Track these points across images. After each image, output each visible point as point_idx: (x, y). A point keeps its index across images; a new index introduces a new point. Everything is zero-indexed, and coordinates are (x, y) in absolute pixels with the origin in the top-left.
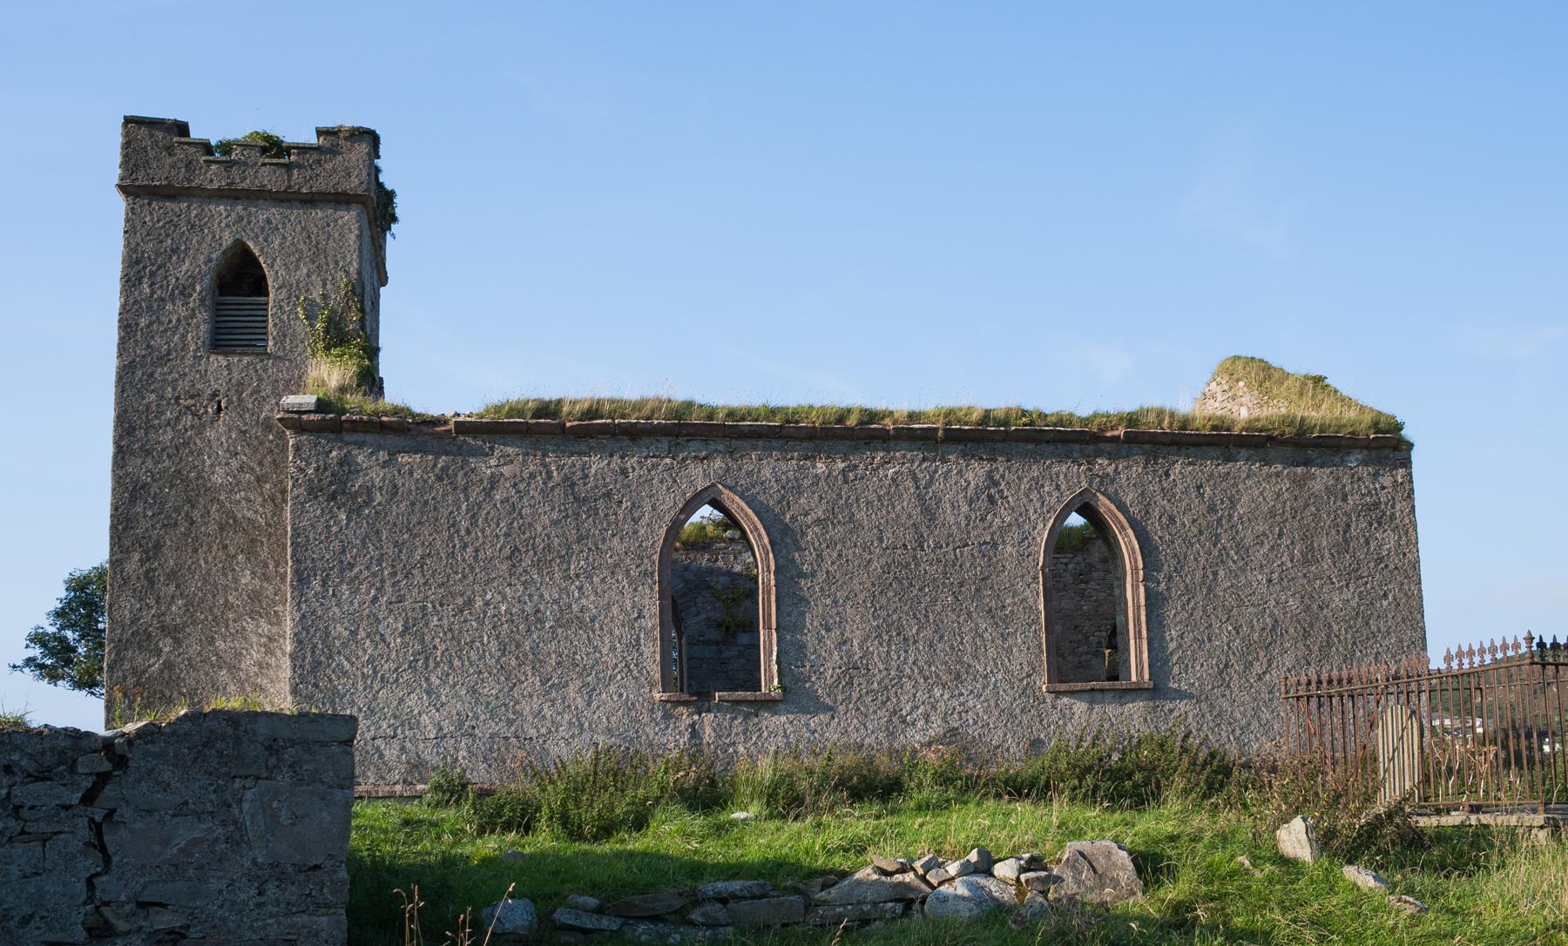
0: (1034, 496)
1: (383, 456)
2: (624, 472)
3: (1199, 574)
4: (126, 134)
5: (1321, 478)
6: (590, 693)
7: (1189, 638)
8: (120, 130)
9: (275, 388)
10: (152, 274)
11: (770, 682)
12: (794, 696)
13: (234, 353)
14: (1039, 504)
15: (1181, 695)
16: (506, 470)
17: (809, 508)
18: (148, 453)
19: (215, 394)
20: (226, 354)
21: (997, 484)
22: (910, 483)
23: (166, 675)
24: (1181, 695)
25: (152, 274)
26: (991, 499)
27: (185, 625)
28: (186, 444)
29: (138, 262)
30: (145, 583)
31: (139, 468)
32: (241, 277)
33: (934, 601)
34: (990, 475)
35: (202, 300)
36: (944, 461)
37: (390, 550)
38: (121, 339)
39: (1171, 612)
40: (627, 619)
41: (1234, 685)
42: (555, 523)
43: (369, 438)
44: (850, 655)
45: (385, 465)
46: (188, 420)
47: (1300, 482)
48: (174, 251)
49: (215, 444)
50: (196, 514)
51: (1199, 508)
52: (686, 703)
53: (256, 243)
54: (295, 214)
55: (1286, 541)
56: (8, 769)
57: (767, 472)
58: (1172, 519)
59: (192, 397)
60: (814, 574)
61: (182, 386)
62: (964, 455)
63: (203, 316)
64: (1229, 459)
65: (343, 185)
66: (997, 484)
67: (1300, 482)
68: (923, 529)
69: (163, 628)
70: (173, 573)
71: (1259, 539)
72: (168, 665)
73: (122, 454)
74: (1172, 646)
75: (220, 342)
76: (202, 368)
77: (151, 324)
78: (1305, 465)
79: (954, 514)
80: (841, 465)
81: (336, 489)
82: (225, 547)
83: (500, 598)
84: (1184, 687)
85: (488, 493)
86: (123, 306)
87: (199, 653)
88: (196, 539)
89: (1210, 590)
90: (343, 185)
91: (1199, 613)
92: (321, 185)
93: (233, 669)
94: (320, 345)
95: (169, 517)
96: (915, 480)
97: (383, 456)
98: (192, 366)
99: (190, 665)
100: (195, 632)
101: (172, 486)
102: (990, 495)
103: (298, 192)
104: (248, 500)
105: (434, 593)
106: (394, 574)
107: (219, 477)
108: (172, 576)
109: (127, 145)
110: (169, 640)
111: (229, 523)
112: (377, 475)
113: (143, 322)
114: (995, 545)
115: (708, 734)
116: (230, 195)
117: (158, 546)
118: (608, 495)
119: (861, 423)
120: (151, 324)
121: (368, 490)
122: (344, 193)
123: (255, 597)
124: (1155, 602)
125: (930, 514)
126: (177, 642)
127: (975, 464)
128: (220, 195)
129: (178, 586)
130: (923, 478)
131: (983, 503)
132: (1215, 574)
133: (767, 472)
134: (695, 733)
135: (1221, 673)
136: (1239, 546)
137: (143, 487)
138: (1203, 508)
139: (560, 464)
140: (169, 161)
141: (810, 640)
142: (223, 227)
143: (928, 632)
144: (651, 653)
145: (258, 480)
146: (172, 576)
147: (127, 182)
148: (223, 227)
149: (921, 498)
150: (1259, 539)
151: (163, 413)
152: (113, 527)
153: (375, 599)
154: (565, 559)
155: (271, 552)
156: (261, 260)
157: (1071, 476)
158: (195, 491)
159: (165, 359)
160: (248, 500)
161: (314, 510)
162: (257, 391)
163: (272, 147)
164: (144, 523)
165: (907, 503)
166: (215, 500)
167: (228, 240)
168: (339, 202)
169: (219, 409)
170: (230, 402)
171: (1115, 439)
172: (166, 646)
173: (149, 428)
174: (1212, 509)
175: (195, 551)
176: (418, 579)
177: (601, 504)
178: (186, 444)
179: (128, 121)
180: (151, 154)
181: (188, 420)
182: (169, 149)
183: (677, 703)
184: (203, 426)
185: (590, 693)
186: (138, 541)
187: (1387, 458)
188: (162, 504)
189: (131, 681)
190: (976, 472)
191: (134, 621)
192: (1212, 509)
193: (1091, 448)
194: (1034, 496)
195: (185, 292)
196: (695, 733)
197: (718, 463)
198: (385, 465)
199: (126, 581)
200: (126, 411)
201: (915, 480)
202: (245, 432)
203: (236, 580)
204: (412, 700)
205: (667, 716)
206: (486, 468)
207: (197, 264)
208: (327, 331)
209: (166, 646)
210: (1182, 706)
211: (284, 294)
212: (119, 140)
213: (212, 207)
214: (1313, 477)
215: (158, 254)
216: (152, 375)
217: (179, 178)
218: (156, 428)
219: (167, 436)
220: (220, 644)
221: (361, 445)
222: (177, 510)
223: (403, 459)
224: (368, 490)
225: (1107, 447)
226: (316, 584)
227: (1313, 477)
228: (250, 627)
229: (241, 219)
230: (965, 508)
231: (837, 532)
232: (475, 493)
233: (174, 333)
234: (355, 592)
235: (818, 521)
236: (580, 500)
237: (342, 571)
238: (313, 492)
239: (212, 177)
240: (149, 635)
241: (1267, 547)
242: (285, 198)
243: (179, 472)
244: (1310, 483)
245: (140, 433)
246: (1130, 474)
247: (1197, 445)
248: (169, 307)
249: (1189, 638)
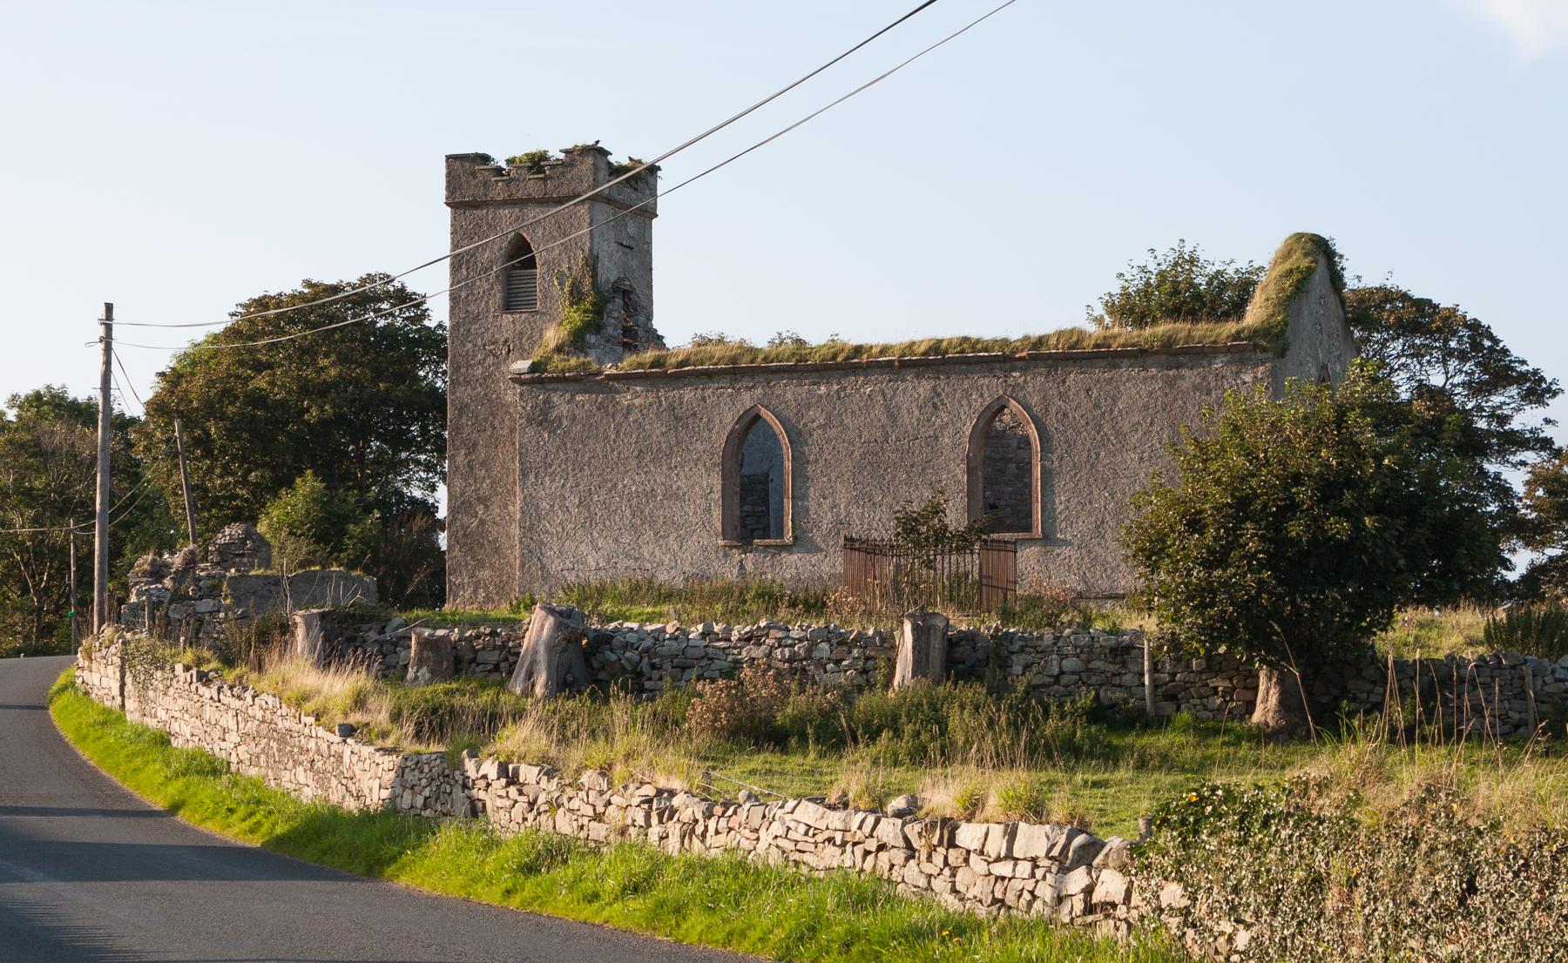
0: (964, 402)
1: (568, 396)
2: (704, 399)
3: (1085, 454)
4: (448, 167)
5: (1190, 377)
6: (681, 541)
7: (1074, 502)
8: (444, 164)
11: (1038, 530)
12: (800, 542)
14: (966, 403)
15: (1067, 543)
16: (637, 402)
17: (816, 416)
18: (468, 383)
21: (939, 395)
22: (880, 398)
24: (1067, 543)
26: (935, 407)
32: (520, 254)
33: (894, 478)
34: (934, 389)
36: (904, 380)
37: (572, 455)
39: (1060, 484)
40: (702, 490)
41: (1109, 536)
42: (663, 434)
43: (560, 386)
44: (838, 514)
45: (569, 402)
46: (490, 360)
47: (1171, 383)
50: (496, 423)
51: (1086, 405)
52: (736, 547)
55: (1156, 428)
56: (1386, 959)
57: (789, 395)
58: (1065, 415)
60: (816, 461)
61: (488, 336)
62: (917, 376)
63: (498, 287)
64: (1115, 367)
66: (939, 395)
67: (1171, 383)
68: (889, 429)
71: (1135, 427)
72: (482, 522)
74: (1062, 507)
75: (509, 306)
78: (1177, 368)
79: (910, 417)
80: (836, 387)
81: (542, 418)
83: (631, 482)
84: (1069, 537)
85: (626, 417)
89: (1092, 466)
91: (1082, 484)
96: (884, 395)
97: (568, 396)
100: (496, 500)
102: (934, 403)
105: (596, 480)
108: (483, 464)
109: (448, 175)
114: (937, 438)
115: (749, 566)
117: (475, 445)
118: (694, 414)
119: (847, 358)
121: (559, 418)
124: (1047, 475)
125: (893, 418)
126: (486, 507)
127: (924, 382)
128: (504, 203)
130: (889, 393)
131: (929, 408)
132: (1098, 454)
133: (789, 395)
134: (742, 567)
135: (1097, 527)
136: (1118, 434)
138: (1090, 405)
139: (668, 395)
141: (812, 505)
142: (507, 223)
143: (889, 499)
144: (717, 513)
146: (483, 464)
148: (507, 223)
149: (887, 407)
150: (1135, 427)
157: (988, 388)
159: (476, 319)
161: (530, 432)
162: (530, 337)
164: (467, 431)
165: (878, 411)
166: (507, 412)
171: (1021, 359)
172: (480, 510)
173: (468, 366)
174: (1097, 406)
176: (587, 472)
177: (690, 421)
179: (448, 157)
181: (490, 360)
182: (474, 174)
183: (731, 547)
185: (681, 541)
186: (463, 442)
187: (1249, 359)
189: (460, 534)
190: (924, 387)
192: (1097, 406)
193: (1008, 365)
194: (964, 402)
196: (742, 567)
198: (569, 402)
201: (884, 395)
204: (582, 547)
205: (726, 555)
206: (625, 399)
207: (494, 244)
208: (571, 293)
209: (480, 510)
210: (1066, 551)
211: (545, 268)
212: (444, 171)
214: (1183, 378)
219: (479, 371)
221: (555, 391)
222: (486, 420)
223: (579, 398)
224: (559, 418)
225: (1020, 364)
226: (532, 477)
227: (1183, 378)
230: (917, 413)
231: (832, 433)
232: (619, 418)
235: (820, 427)
236: (677, 418)
238: (530, 421)
239: (499, 191)
241: (1140, 433)
242: (544, 202)
244: (1180, 382)
245: (463, 370)
246: (1035, 384)
249: (1074, 502)
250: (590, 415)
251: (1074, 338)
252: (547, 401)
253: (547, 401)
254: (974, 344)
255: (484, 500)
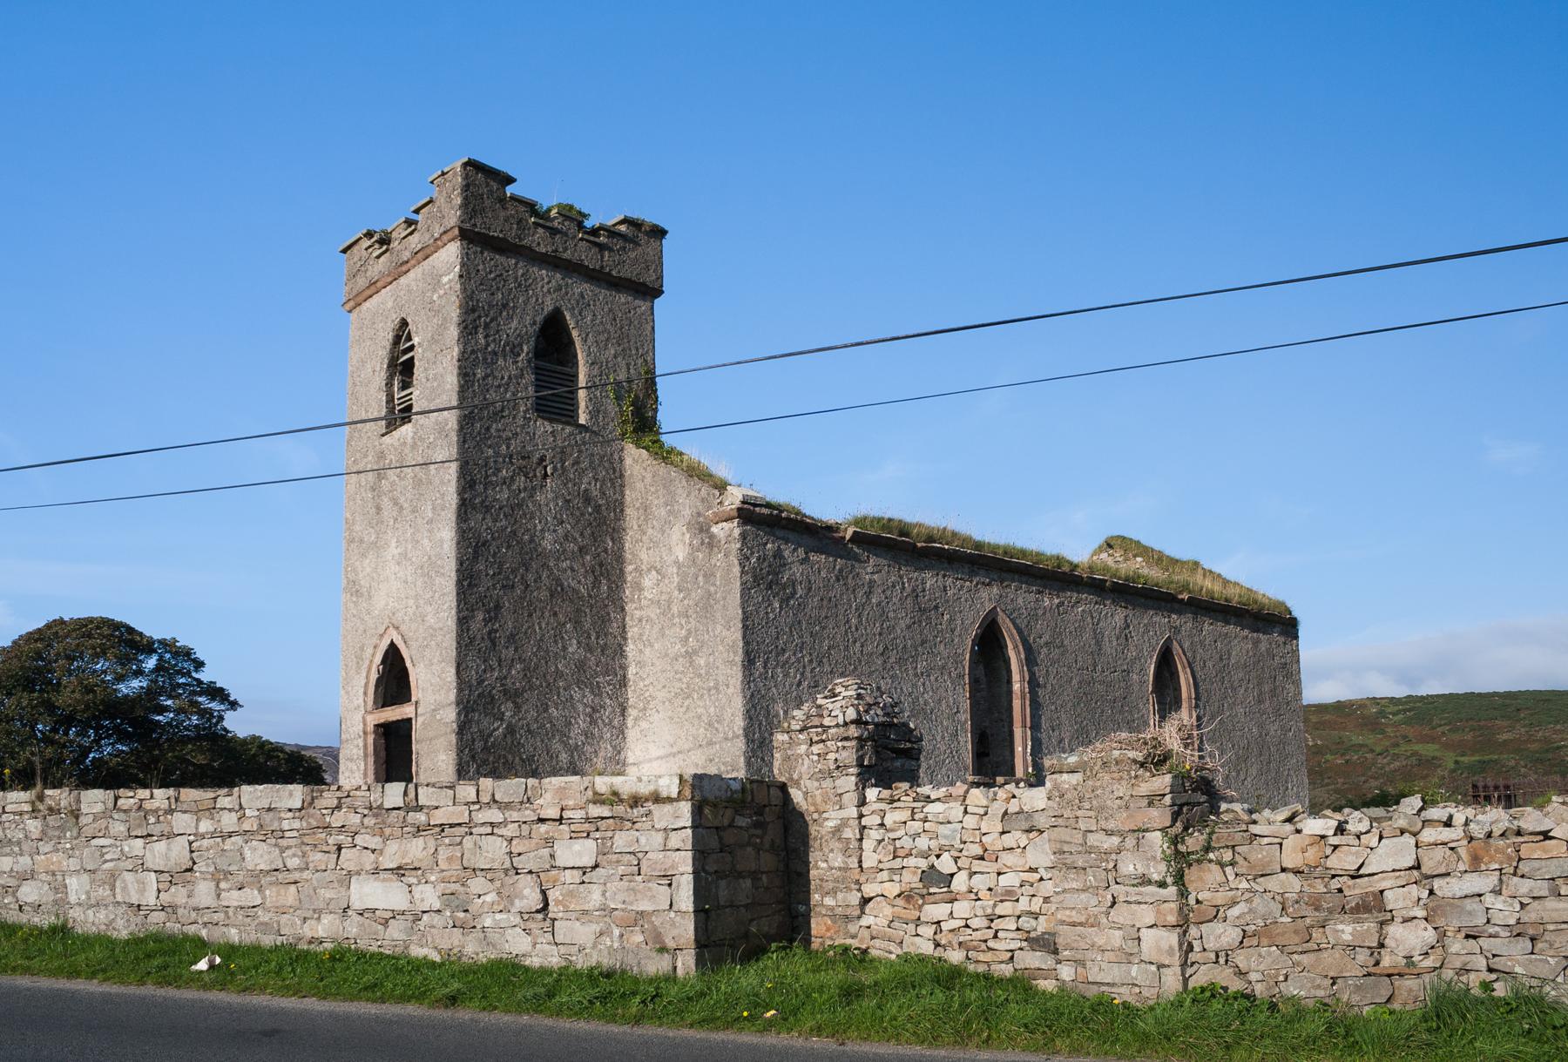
9: (591, 462)
10: (487, 326)
13: (559, 421)
18: (488, 509)
19: (542, 459)
20: (551, 421)
23: (509, 739)
25: (487, 326)
27: (524, 691)
28: (520, 506)
29: (473, 310)
30: (488, 643)
31: (475, 519)
32: (553, 342)
35: (529, 361)
37: (807, 639)
38: (461, 386)
46: (521, 481)
47: (1256, 643)
48: (505, 306)
49: (545, 509)
50: (530, 577)
53: (573, 315)
54: (603, 293)
59: (523, 458)
65: (624, 264)
67: (1256, 643)
69: (505, 692)
70: (512, 636)
72: (511, 730)
73: (465, 509)
76: (531, 430)
77: (487, 376)
80: (1057, 601)
82: (555, 614)
85: (868, 594)
86: (463, 353)
87: (536, 720)
88: (530, 603)
90: (624, 264)
92: (627, 272)
93: (565, 736)
94: (630, 428)
95: (507, 578)
98: (523, 427)
99: (529, 731)
100: (532, 697)
101: (508, 547)
103: (609, 274)
104: (573, 570)
106: (811, 661)
107: (548, 543)
108: (512, 638)
110: (510, 705)
111: (558, 591)
112: (797, 571)
113: (480, 373)
116: (553, 262)
117: (498, 607)
118: (936, 607)
120: (487, 376)
121: (793, 583)
122: (644, 284)
123: (581, 666)
126: (518, 707)
129: (516, 650)
137: (484, 545)
139: (911, 576)
140: (502, 214)
142: (546, 291)
145: (581, 549)
147: (467, 226)
151: (499, 470)
152: (459, 583)
153: (799, 684)
154: (915, 659)
155: (593, 624)
156: (575, 333)
158: (530, 555)
159: (498, 415)
160: (573, 570)
163: (574, 217)
167: (549, 307)
168: (637, 292)
169: (546, 475)
170: (555, 469)
172: (508, 710)
175: (530, 615)
176: (827, 668)
178: (520, 506)
180: (487, 203)
184: (534, 488)
188: (501, 565)
189: (479, 745)
191: (480, 682)
195: (515, 351)
197: (995, 590)
199: (472, 640)
200: (467, 463)
202: (568, 501)
203: (564, 648)
207: (522, 324)
209: (508, 710)
213: (535, 269)
215: (491, 306)
216: (488, 429)
217: (512, 234)
218: (494, 485)
220: (552, 710)
221: (787, 541)
223: (813, 557)
225: (1176, 606)
228: (577, 696)
229: (559, 289)
233: (506, 391)
234: (786, 675)
237: (778, 655)
240: (493, 698)
243: (514, 532)
247: (1158, 599)
248: (501, 362)
250: (828, 586)
251: (830, 529)
252: (778, 554)
253: (778, 554)
254: (904, 529)
255: (513, 696)
